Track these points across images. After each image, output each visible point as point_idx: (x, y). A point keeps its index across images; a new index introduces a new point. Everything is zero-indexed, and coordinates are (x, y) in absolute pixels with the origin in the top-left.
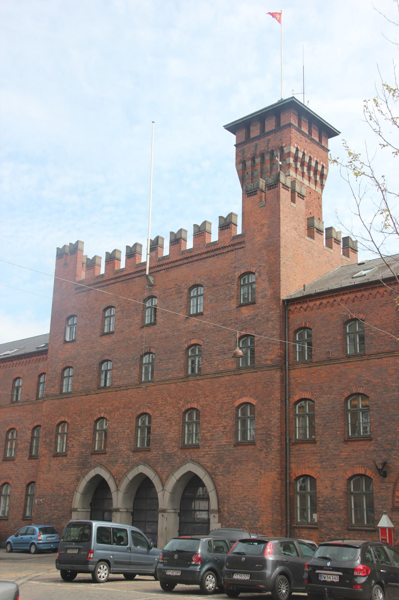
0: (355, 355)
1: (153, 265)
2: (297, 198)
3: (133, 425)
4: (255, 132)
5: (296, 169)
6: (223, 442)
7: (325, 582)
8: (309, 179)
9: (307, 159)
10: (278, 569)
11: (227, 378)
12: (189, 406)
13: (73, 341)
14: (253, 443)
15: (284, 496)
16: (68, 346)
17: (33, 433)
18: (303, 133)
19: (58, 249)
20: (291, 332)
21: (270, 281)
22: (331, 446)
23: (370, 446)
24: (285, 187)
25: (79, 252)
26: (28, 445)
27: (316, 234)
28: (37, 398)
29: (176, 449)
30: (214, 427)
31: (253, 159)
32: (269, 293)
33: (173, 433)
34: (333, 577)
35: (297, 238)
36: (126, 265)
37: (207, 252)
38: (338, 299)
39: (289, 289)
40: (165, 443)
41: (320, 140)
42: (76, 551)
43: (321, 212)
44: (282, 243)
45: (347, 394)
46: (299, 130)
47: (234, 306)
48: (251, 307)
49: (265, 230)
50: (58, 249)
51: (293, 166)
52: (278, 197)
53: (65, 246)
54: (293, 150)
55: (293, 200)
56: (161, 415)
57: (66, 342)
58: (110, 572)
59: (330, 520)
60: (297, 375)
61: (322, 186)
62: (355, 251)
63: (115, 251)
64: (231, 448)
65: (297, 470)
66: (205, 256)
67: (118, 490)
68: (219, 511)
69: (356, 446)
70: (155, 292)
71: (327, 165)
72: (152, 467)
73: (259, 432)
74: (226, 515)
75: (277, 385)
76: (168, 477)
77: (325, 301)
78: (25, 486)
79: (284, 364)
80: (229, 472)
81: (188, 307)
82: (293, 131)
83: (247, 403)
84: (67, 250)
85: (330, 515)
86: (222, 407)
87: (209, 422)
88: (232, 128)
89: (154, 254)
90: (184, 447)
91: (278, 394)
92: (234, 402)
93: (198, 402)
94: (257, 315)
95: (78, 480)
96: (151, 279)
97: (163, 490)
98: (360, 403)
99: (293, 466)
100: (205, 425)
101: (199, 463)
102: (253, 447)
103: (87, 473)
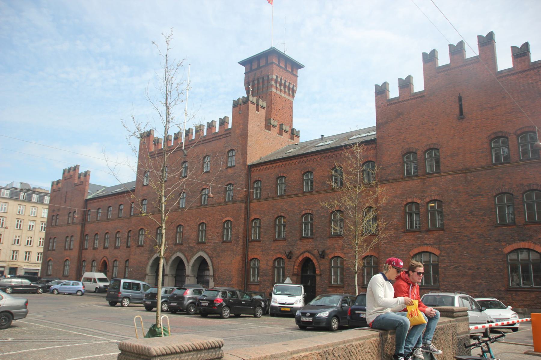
0: (282, 196)
1: (187, 144)
2: (260, 109)
3: (175, 231)
4: (255, 66)
5: (277, 88)
6: (217, 241)
7: (203, 306)
8: (285, 93)
9: (283, 82)
10: (191, 301)
11: (220, 207)
12: (201, 221)
13: (147, 185)
14: (230, 242)
15: (244, 269)
16: (145, 188)
17: (128, 234)
18: (281, 67)
19: (234, 101)
20: (252, 182)
21: (242, 155)
22: (267, 243)
23: (285, 243)
24: (252, 103)
25: (151, 136)
26: (126, 240)
27: (272, 128)
28: (97, 220)
29: (195, 244)
30: (213, 233)
31: (253, 81)
32: (241, 161)
33: (194, 236)
34: (206, 304)
35: (259, 130)
36: (232, 126)
37: (213, 138)
38: (274, 165)
39: (253, 158)
40: (190, 241)
41: (292, 71)
42: (113, 293)
43: (292, 112)
44: (249, 134)
45: (276, 216)
46: (278, 65)
47: (225, 168)
48: (232, 169)
49: (241, 126)
50: (234, 101)
51: (275, 85)
52: (248, 108)
53: (239, 99)
54: (274, 77)
55: (257, 110)
56: (188, 226)
57: (144, 185)
58: (130, 303)
59: (265, 281)
60: (254, 205)
61: (293, 97)
62: (298, 136)
63: (212, 121)
64: (220, 244)
65: (251, 256)
66: (212, 140)
67: (167, 265)
68: (214, 276)
69: (279, 243)
70: (187, 159)
71: (297, 84)
72: (183, 253)
73: (234, 236)
74: (217, 278)
75: (243, 211)
76: (190, 259)
77: (268, 166)
78: (124, 262)
79: (247, 199)
80: (219, 257)
81: (227, 163)
82: (275, 66)
83: (229, 220)
84: (241, 101)
85: (265, 278)
86: (217, 222)
87: (210, 230)
88: (243, 63)
89: (187, 138)
90: (199, 243)
91: (243, 216)
92: (222, 220)
93: (206, 219)
94: (235, 173)
95: (149, 259)
96: (185, 152)
97: (188, 265)
98: (339, 216)
99: (249, 253)
100: (208, 232)
101: (205, 252)
102: (230, 243)
103: (153, 256)
